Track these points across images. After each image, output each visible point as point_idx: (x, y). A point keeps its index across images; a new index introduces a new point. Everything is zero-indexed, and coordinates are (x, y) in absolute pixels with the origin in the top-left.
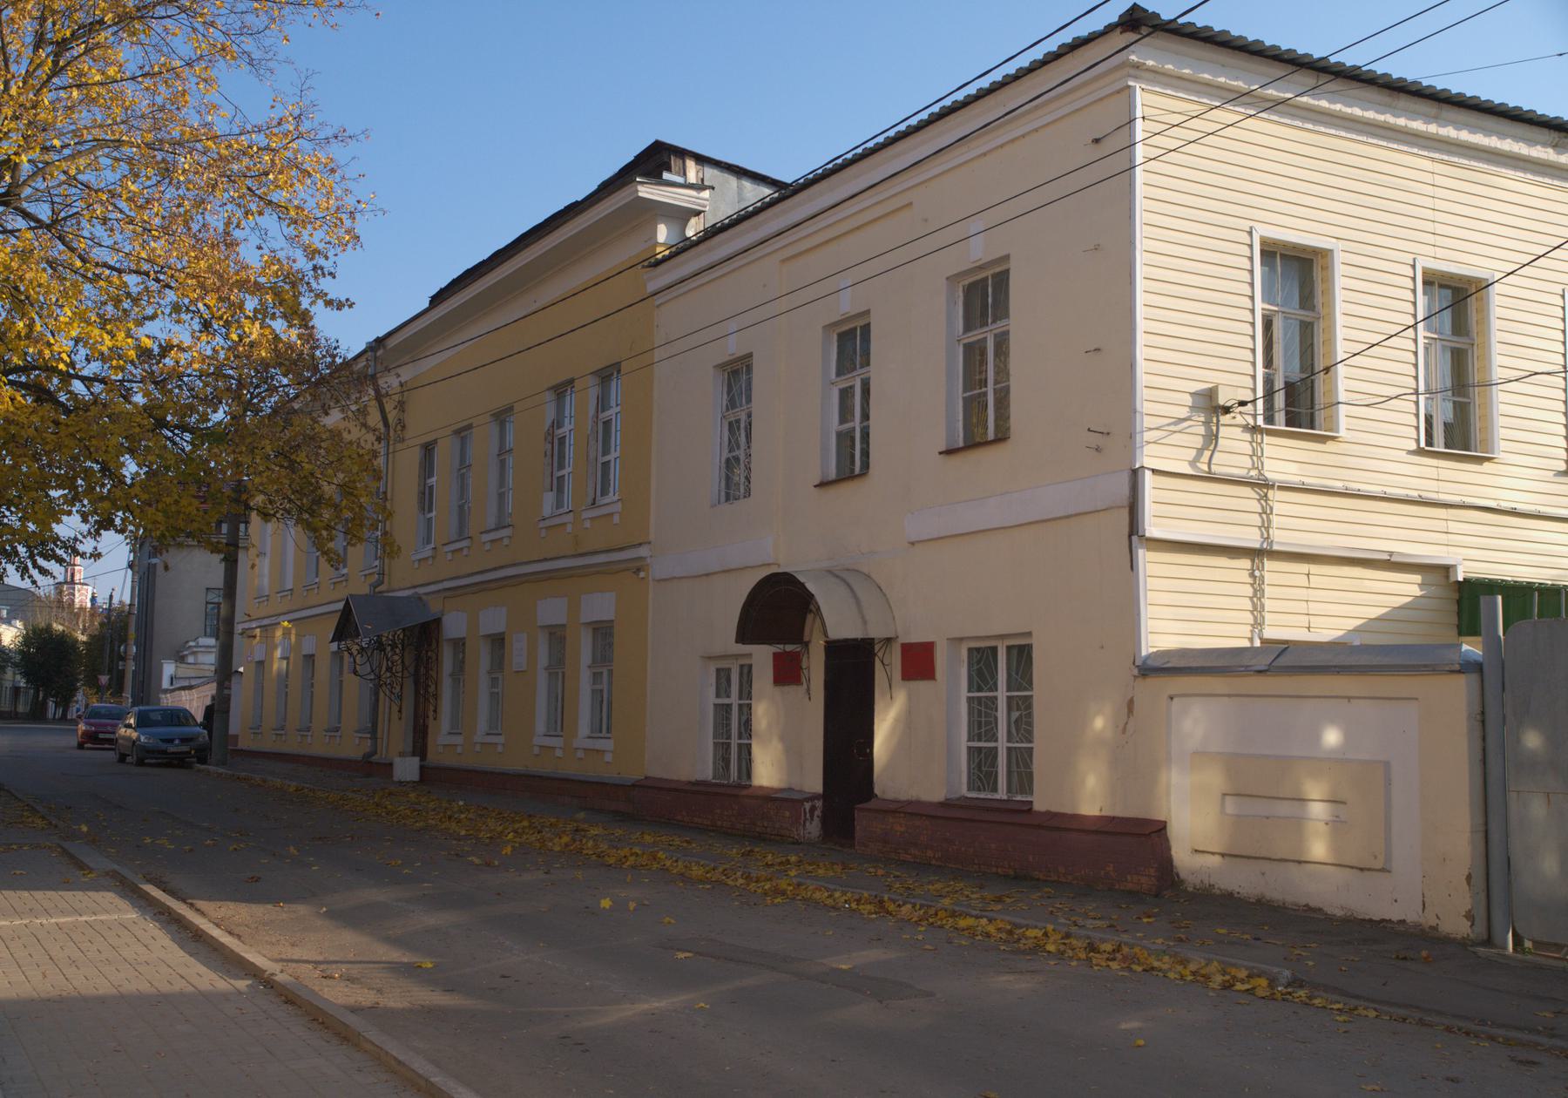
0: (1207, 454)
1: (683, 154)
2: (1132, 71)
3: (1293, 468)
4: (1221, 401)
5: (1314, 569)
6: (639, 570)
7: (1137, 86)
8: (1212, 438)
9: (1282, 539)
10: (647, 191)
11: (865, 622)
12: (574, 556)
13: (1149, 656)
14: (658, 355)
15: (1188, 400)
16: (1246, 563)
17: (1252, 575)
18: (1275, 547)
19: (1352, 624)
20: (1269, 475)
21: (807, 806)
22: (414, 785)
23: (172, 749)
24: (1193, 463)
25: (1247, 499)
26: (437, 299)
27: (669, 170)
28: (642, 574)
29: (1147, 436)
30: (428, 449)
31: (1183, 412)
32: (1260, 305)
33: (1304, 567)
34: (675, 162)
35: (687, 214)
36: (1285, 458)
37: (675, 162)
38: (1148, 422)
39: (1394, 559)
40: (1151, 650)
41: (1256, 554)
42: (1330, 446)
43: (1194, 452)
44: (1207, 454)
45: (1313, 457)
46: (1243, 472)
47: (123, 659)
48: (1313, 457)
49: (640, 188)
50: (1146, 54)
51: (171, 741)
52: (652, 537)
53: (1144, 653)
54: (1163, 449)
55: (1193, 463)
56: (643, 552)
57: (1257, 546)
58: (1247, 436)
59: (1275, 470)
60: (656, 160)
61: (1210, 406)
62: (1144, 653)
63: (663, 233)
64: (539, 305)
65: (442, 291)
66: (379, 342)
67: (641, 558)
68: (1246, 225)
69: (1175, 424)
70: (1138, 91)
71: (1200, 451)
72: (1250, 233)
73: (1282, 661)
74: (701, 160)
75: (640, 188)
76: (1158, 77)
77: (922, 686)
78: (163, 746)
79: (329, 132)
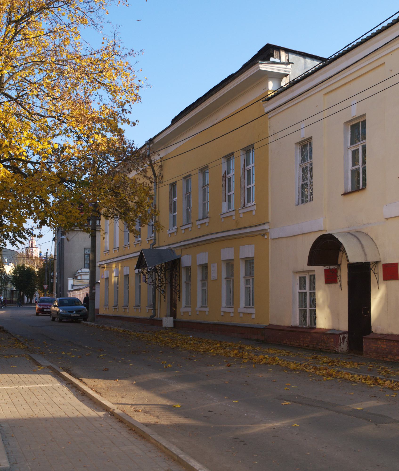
1: (279, 49)
6: (264, 235)
10: (263, 67)
11: (366, 255)
21: (341, 337)
26: (175, 121)
27: (273, 56)
28: (266, 237)
30: (173, 186)
34: (276, 53)
37: (276, 53)
47: (53, 278)
51: (72, 312)
52: (270, 220)
56: (266, 227)
63: (271, 85)
64: (216, 122)
66: (151, 140)
75: (260, 66)
78: (69, 314)
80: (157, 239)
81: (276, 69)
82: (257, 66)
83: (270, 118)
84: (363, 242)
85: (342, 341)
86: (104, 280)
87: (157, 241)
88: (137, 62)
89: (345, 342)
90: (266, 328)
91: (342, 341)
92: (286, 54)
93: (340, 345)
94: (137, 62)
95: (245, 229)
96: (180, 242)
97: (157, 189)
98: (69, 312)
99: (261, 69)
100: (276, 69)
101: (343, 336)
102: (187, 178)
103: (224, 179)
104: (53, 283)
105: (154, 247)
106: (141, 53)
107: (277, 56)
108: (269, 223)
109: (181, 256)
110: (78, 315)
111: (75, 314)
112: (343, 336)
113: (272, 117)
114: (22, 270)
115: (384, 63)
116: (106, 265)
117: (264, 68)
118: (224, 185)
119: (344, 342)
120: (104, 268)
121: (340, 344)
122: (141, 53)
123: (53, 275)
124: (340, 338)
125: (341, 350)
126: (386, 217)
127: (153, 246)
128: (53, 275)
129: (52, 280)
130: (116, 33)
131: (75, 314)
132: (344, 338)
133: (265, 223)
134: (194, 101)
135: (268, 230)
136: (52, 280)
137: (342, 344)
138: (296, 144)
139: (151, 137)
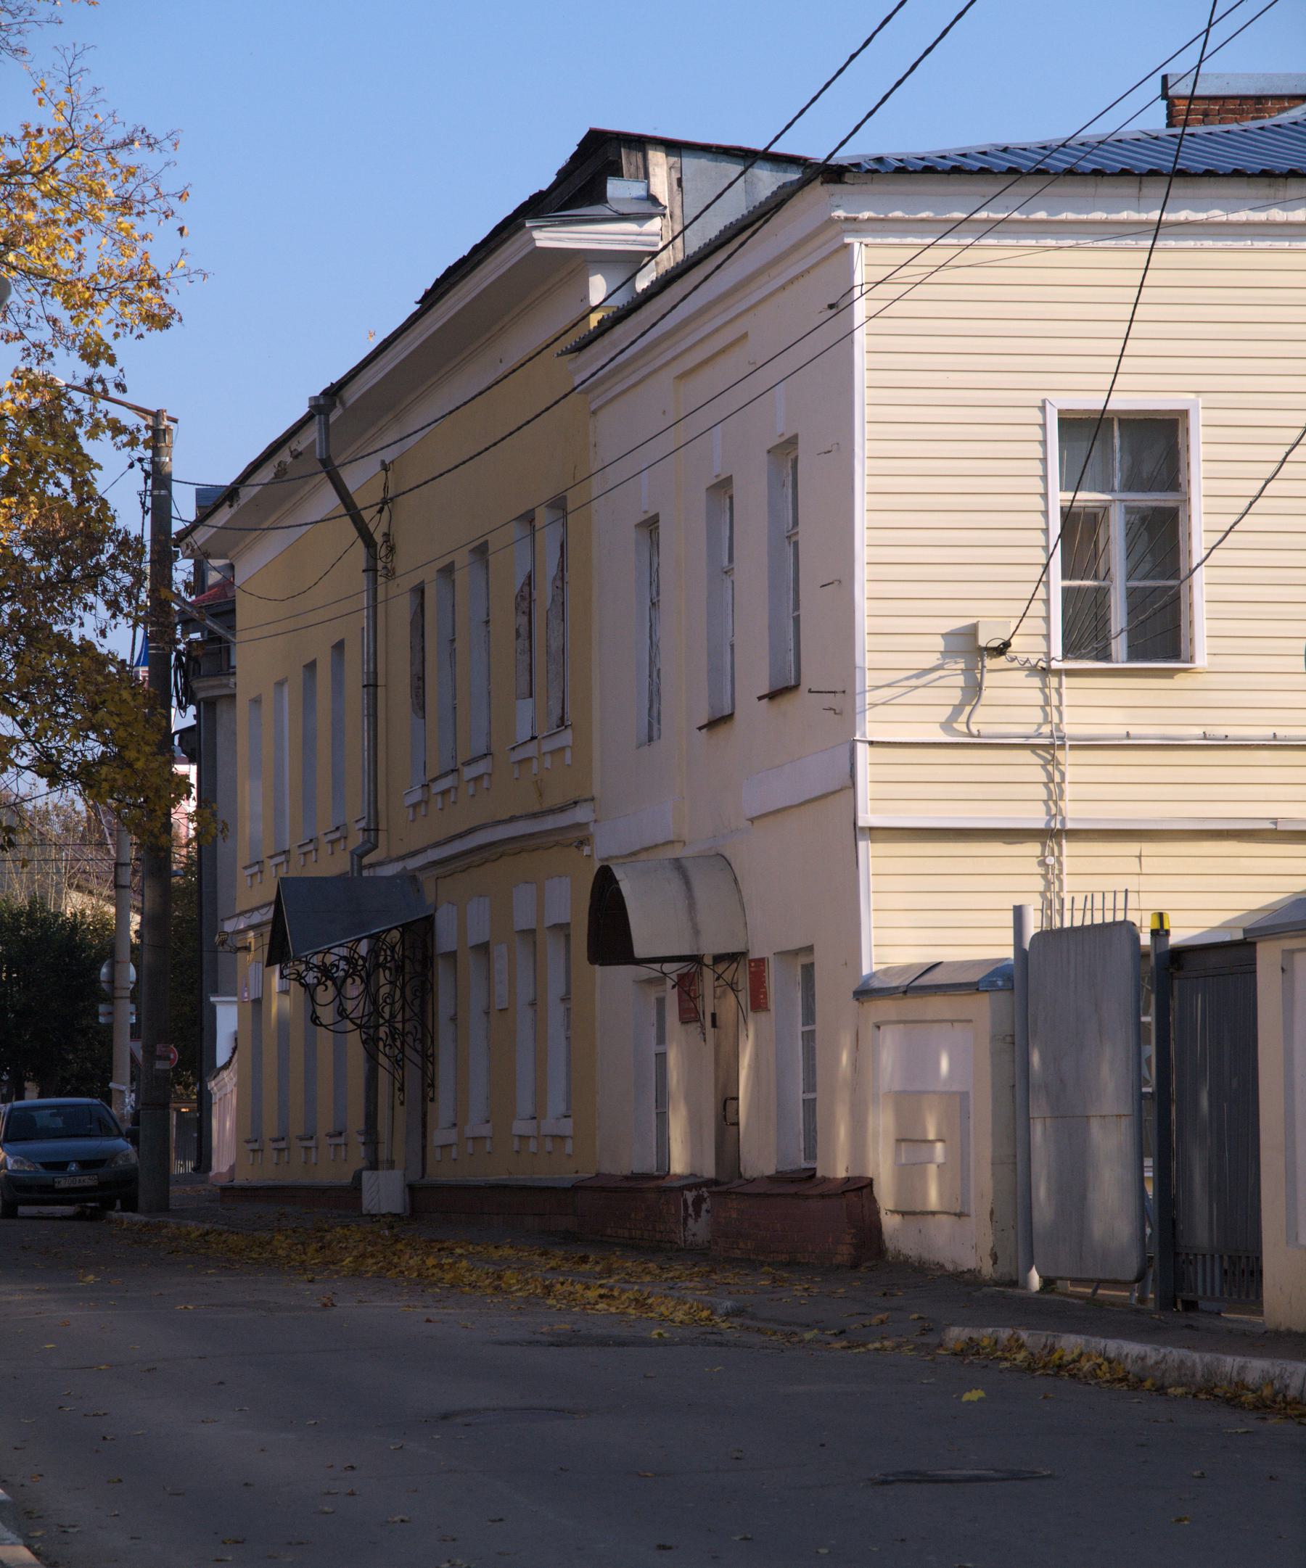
0: (968, 709)
1: (641, 143)
2: (845, 226)
3: (1118, 715)
4: (982, 642)
5: (1148, 848)
6: (582, 843)
7: (854, 241)
8: (974, 690)
9: (1075, 814)
10: (548, 237)
11: (696, 932)
12: (534, 816)
13: (873, 975)
14: (596, 486)
15: (940, 644)
16: (1034, 848)
17: (1043, 863)
18: (1069, 826)
19: (1217, 919)
20: (1067, 730)
21: (690, 1196)
22: (393, 1220)
23: (63, 1182)
24: (947, 725)
25: (1029, 768)
26: (430, 299)
27: (618, 173)
28: (586, 850)
29: (870, 697)
30: (419, 591)
31: (933, 660)
32: (1059, 497)
33: (1133, 848)
34: (628, 160)
35: (634, 261)
36: (1102, 703)
37: (628, 160)
38: (870, 679)
39: (1280, 827)
40: (875, 968)
41: (1049, 835)
42: (1180, 680)
43: (949, 710)
44: (968, 709)
45: (1150, 699)
46: (1030, 730)
47: (110, 999)
48: (1150, 699)
49: (536, 234)
50: (841, 205)
51: (60, 1166)
52: (596, 792)
53: (865, 971)
54: (896, 707)
55: (947, 725)
56: (580, 814)
57: (1041, 825)
58: (1036, 681)
59: (1075, 723)
60: (595, 166)
61: (973, 651)
62: (865, 971)
63: (598, 288)
64: (503, 369)
65: (428, 294)
66: (334, 393)
67: (578, 826)
68: (1036, 398)
69: (917, 676)
70: (857, 246)
71: (958, 709)
72: (1043, 409)
73: (926, 980)
74: (673, 147)
75: (536, 234)
76: (882, 225)
77: (762, 1016)
78: (46, 1175)
79: (119, 134)
80: (382, 826)
81: (600, 241)
82: (526, 237)
83: (594, 413)
84: (699, 892)
85: (691, 1210)
86: (249, 1006)
87: (382, 835)
88: (167, 164)
89: (703, 1213)
90: (576, 1188)
91: (691, 1210)
92: (673, 159)
93: (685, 1224)
94: (167, 164)
95: (470, 837)
96: (423, 850)
97: (381, 608)
98: (46, 1166)
99: (539, 244)
100: (600, 241)
101: (694, 1193)
102: (447, 571)
103: (525, 605)
104: (109, 1028)
105: (366, 861)
106: (167, 145)
107: (633, 169)
108: (593, 799)
109: (436, 910)
110: (88, 1180)
111: (72, 1175)
112: (694, 1193)
113: (601, 408)
114: (25, 940)
115: (745, 336)
116: (251, 934)
117: (551, 239)
118: (523, 631)
119: (698, 1214)
120: (247, 949)
121: (685, 1220)
122: (167, 145)
123: (112, 981)
124: (685, 1201)
125: (690, 1238)
126: (749, 816)
127: (361, 857)
128: (112, 981)
129: (102, 1008)
130: (75, 69)
131: (72, 1175)
132: (698, 1201)
133: (576, 803)
134: (510, 212)
135: (592, 828)
136: (102, 1008)
137: (691, 1222)
138: (638, 526)
139: (336, 377)
